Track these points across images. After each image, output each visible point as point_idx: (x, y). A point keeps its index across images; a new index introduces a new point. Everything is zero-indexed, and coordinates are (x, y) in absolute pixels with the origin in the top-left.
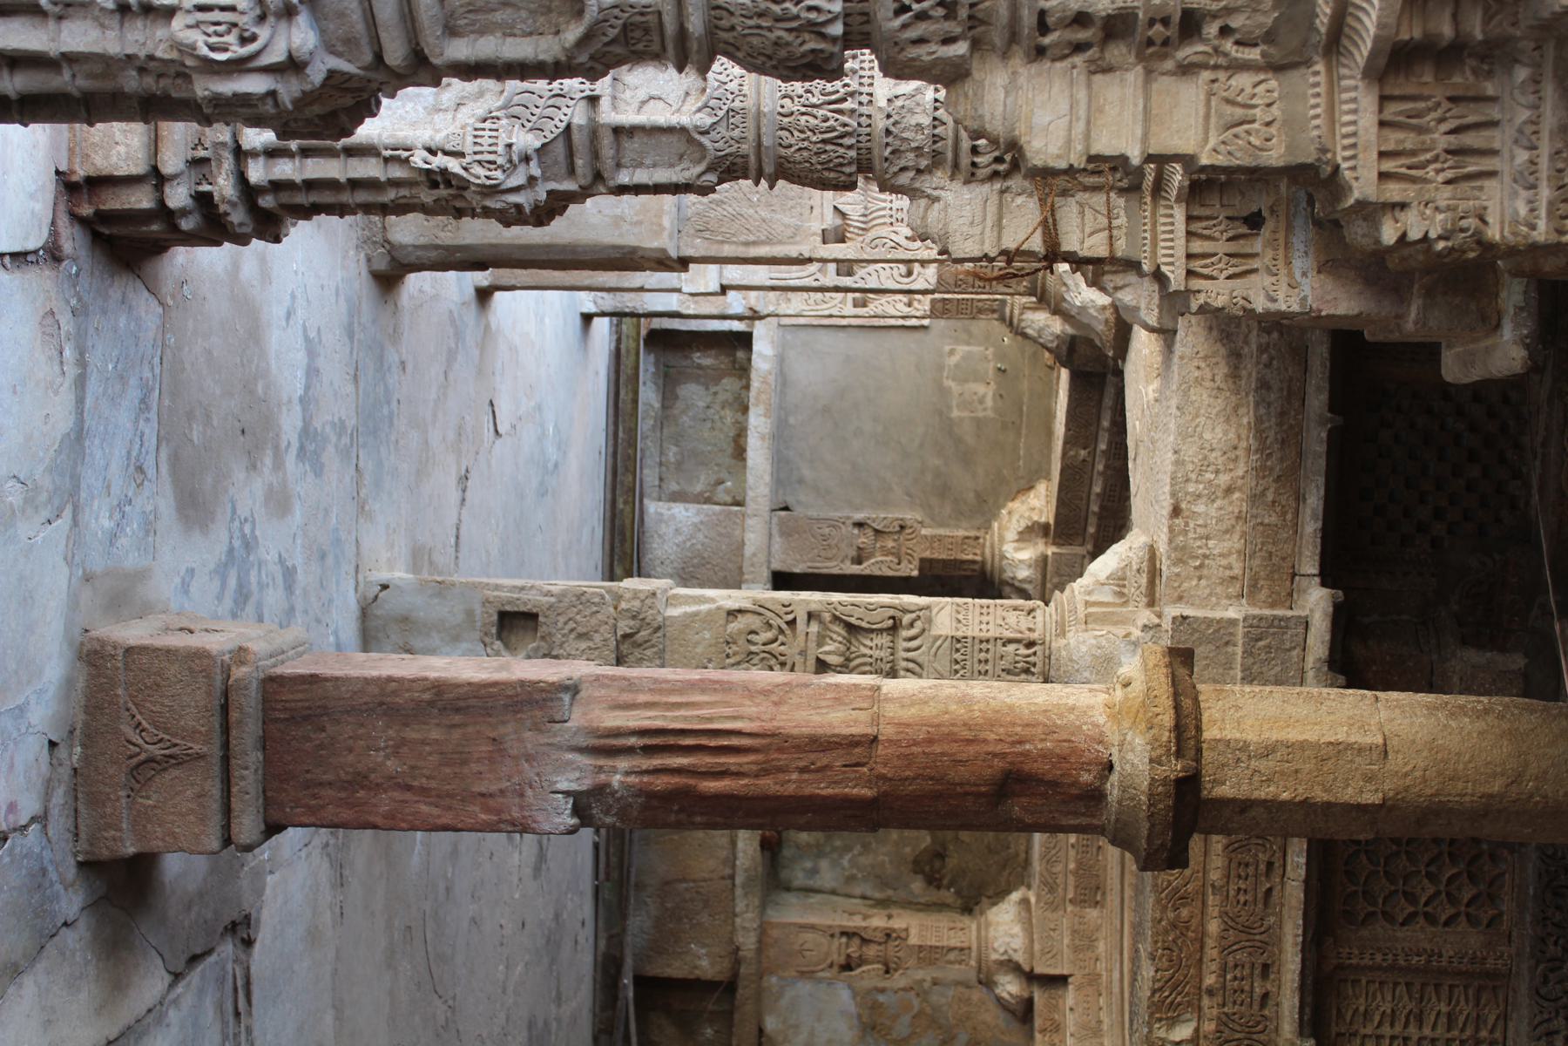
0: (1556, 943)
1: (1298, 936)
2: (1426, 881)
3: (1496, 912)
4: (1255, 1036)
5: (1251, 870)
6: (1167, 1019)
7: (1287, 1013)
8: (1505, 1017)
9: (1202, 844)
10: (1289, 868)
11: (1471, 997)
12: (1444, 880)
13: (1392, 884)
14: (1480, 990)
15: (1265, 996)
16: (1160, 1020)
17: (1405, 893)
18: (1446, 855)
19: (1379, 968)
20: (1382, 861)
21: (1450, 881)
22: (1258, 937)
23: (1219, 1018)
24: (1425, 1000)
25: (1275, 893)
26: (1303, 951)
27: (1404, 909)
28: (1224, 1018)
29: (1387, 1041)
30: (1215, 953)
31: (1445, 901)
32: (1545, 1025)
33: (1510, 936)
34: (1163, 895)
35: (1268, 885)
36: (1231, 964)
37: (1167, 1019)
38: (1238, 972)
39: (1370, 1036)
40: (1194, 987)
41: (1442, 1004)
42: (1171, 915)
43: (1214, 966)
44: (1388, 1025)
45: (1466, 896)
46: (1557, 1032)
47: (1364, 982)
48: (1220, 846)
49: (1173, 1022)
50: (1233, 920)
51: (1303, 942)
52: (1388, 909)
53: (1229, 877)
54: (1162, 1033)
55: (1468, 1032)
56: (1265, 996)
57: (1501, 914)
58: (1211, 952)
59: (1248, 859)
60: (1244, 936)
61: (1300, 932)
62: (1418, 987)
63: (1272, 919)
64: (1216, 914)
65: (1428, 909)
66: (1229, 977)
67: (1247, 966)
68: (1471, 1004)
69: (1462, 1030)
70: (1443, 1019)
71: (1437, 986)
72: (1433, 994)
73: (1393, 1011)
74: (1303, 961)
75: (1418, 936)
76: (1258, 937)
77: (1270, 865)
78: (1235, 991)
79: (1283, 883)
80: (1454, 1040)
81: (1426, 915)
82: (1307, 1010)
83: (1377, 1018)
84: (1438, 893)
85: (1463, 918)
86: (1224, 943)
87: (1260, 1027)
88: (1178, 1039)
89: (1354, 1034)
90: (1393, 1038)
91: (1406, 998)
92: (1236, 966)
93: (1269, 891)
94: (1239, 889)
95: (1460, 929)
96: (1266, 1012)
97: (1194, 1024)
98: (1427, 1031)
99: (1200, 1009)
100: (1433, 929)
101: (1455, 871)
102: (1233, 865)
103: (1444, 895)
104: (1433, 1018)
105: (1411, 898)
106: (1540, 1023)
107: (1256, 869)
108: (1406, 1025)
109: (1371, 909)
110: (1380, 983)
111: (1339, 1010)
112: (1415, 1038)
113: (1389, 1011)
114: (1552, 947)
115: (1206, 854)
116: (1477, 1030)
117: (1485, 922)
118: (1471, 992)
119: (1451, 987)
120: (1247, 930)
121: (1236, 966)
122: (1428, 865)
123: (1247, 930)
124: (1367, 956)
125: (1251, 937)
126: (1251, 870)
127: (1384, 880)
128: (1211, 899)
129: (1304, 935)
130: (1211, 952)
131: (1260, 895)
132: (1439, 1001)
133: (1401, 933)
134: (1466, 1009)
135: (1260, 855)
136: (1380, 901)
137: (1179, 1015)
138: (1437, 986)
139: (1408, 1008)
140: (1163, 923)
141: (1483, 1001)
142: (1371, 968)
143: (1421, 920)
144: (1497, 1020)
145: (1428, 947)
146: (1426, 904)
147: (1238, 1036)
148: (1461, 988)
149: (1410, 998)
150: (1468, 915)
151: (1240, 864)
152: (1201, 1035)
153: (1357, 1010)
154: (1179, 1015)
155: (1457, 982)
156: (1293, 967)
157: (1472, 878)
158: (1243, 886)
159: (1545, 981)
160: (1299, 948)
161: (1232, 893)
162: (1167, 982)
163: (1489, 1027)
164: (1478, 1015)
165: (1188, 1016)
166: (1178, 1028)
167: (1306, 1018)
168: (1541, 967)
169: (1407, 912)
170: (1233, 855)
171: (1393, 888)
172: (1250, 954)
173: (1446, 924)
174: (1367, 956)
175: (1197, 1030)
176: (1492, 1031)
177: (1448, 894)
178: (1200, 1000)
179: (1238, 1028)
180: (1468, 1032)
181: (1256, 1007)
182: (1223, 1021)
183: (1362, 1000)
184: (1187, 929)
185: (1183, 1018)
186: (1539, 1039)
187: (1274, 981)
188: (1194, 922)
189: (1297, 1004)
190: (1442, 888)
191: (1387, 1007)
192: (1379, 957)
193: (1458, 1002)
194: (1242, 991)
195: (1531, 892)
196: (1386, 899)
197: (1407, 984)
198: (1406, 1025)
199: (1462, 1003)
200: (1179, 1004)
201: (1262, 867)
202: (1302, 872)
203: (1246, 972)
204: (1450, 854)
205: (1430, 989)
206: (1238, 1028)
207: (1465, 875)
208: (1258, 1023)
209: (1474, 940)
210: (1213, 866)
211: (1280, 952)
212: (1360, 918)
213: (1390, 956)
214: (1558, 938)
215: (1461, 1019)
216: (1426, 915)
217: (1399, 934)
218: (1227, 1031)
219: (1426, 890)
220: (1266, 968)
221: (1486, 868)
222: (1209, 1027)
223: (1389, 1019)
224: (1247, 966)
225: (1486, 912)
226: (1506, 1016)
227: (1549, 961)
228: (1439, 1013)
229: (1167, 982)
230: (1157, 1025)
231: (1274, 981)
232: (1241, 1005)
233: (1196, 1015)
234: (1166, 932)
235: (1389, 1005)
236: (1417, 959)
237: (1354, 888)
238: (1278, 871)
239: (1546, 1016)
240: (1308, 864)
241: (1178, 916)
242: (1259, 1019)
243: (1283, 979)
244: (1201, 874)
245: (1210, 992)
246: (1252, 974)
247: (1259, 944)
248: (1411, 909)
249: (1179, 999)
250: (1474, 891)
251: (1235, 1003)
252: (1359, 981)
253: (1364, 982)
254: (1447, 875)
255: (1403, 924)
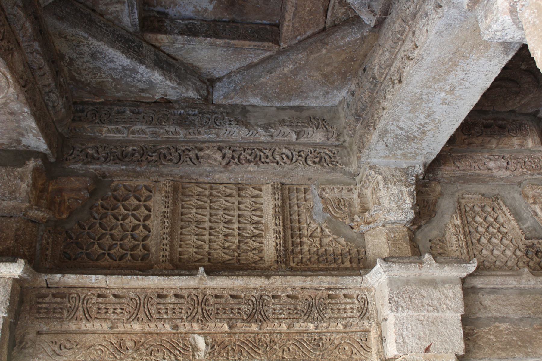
0: (152, 156)
1: (137, 278)
2: (126, 221)
3: (144, 188)
4: (200, 301)
5: (102, 306)
6: (193, 352)
7: (184, 283)
8: (198, 183)
9: (87, 335)
10: (101, 285)
11: (188, 199)
12: (126, 212)
13: (127, 237)
14: (183, 194)
15: (176, 296)
16: (194, 356)
17: (132, 231)
18: (113, 212)
19: (171, 242)
20: (114, 242)
21: (126, 209)
22: (142, 301)
23: (190, 321)
24: (190, 220)
25: (116, 292)
26: (146, 275)
27: (141, 232)
28: (190, 318)
29: (212, 237)
30: (152, 325)
31: (137, 212)
32: (193, 160)
33: (156, 182)
34: (118, 357)
35: (111, 296)
36: (158, 316)
37: (193, 352)
38: (163, 311)
39: (209, 245)
40: (174, 336)
41: (192, 212)
42: (130, 352)
43: (160, 325)
44: (203, 237)
45: (136, 202)
46: (197, 155)
47: (180, 250)
48: (88, 325)
49: (195, 348)
50: (132, 316)
51: (141, 275)
52: (141, 239)
53: (106, 319)
54: (202, 354)
55: (206, 199)
56: (176, 296)
57: (145, 186)
58: (152, 327)
59: (95, 308)
60: (142, 309)
61: (135, 277)
62: (183, 223)
63: (131, 293)
64: (128, 326)
65: (142, 219)
66: (165, 317)
67: (159, 306)
68: (191, 198)
69: (205, 202)
70: (200, 211)
71: (182, 214)
72: (186, 216)
73: (196, 235)
74: (153, 275)
75: (155, 224)
76: (142, 301)
77: (99, 296)
78: (174, 313)
79: (111, 289)
80: (210, 206)
81: (144, 220)
82: (183, 272)
83: (200, 243)
84: (133, 215)
85: (147, 203)
86: (145, 319)
87: (195, 298)
88: (205, 345)
89: (209, 254)
90: (210, 234)
91: (189, 229)
92: (159, 313)
93: (115, 296)
94: (114, 313)
95: (152, 204)
96: (186, 295)
97: (196, 336)
98: (207, 218)
99: (187, 333)
100: (152, 217)
101: (121, 207)
102: (99, 316)
103: (134, 212)
104: (199, 216)
105: (135, 228)
106: (192, 162)
107: (101, 303)
108: (204, 229)
109: (141, 247)
110: (181, 241)
111: (195, 262)
112: (210, 224)
113: (196, 237)
114: (153, 158)
115: (94, 333)
116: (205, 195)
117: (149, 193)
118: (185, 199)
119: (183, 208)
120: (137, 308)
121: (159, 313)
122: (118, 220)
123: (137, 308)
124: (165, 247)
125: (142, 305)
126: (102, 306)
127: (126, 241)
128: (121, 329)
129: (137, 275)
130: (152, 327)
131: (117, 301)
132: (191, 213)
133: (154, 231)
134: (194, 201)
135: (93, 301)
136: (136, 243)
137: (191, 345)
138: (182, 214)
139: (195, 228)
140: (135, 356)
141: (191, 193)
142: (172, 246)
143: (147, 223)
144: (199, 187)
145: (160, 218)
146: (139, 221)
147: (200, 311)
148: (183, 203)
149: (189, 227)
150: (145, 201)
151: (98, 313)
152: (201, 331)
153: (195, 253)
154: (191, 345)
155: (180, 205)
156: (156, 280)
157: (126, 199)
158: (112, 310)
159: (171, 160)
160: (144, 277)
161: (116, 317)
162: (171, 352)
163: (203, 190)
164: (198, 195)
165: (191, 340)
166: (199, 345)
167: (187, 273)
168: (163, 162)
169: (143, 230)
170: (93, 317)
171: (130, 237)
172: (152, 305)
173: (150, 211)
174: (165, 247)
175: (199, 334)
176: (206, 189)
177: (134, 210)
178: (181, 333)
179: (196, 310)
180: (206, 199)
181: (182, 301)
182: (191, 318)
183: (190, 250)
184: (139, 342)
185: (193, 343)
186: (200, 162)
187: (167, 291)
188: (135, 338)
189: (177, 277)
190: (130, 213)
191: (194, 238)
192: (165, 242)
193: (191, 204)
194: (174, 309)
195: (124, 167)
196: (135, 239)
197: (181, 228)
198: (204, 229)
199: (191, 202)
200: (185, 345)
201: (100, 300)
202: (100, 277)
203: (161, 306)
204: (112, 210)
205: (184, 217)
206: (196, 310)
207: (124, 202)
208: (192, 299)
209: (158, 197)
210: (100, 328)
211: (150, 288)
212: (146, 252)
213: (165, 236)
214: (148, 155)
215: (199, 203)
216: (144, 220)
217: (154, 233)
218: (197, 317)
219: (131, 221)
220: (159, 296)
221: (121, 193)
222: (196, 327)
223: (200, 237)
224: (159, 306)
225: (144, 193)
226: (197, 183)
227: (160, 159)
228: (196, 213)
229: (171, 352)
230: (197, 357)
231: (167, 291)
232: (182, 309)
233: (190, 335)
234: (141, 354)
235: (193, 236)
236: (166, 223)
237: (129, 256)
238: (103, 292)
239: (188, 159)
240: (96, 274)
241: (131, 347)
242: (189, 299)
243: (166, 286)
244: (106, 336)
245: (176, 327)
246: (164, 304)
247: (146, 301)
248: (141, 227)
249: (181, 345)
250: (133, 198)
251: (181, 313)
252: (180, 251)
253: (180, 250)
254: (124, 211)
255: (150, 232)
